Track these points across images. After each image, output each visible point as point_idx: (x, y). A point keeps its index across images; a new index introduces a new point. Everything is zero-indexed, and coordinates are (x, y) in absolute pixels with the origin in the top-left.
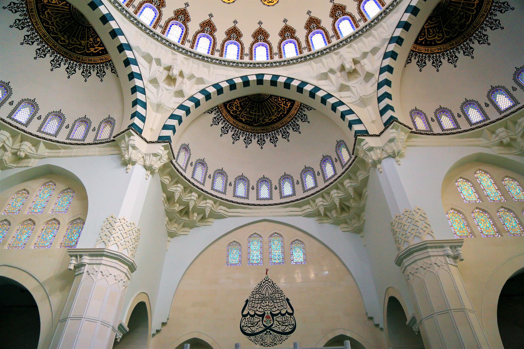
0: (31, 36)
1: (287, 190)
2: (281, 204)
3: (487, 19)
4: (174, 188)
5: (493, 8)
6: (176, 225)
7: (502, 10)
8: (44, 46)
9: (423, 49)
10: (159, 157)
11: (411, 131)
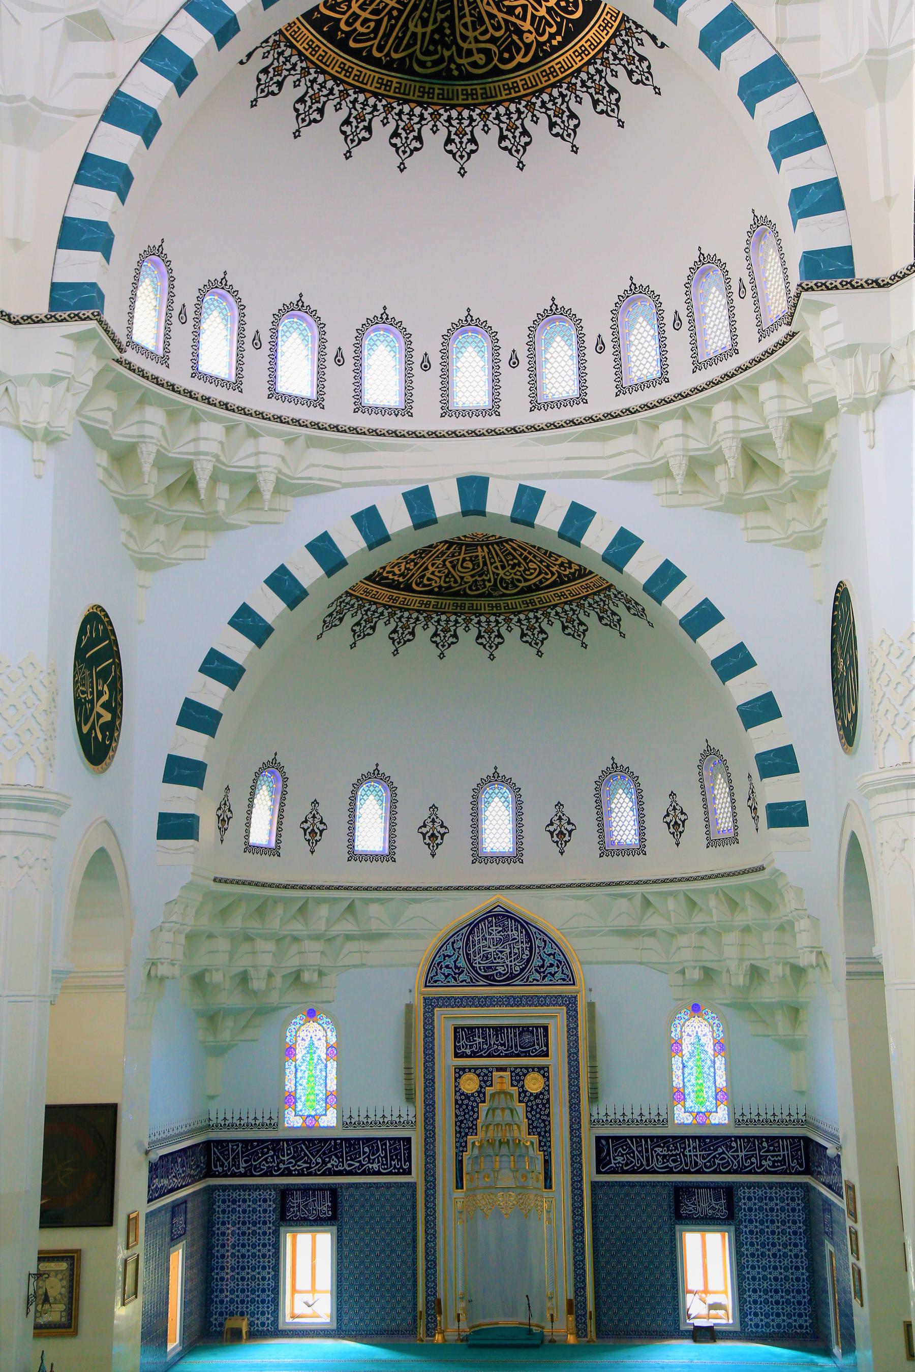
0: (440, 628)
1: (559, 374)
2: (534, 428)
3: (531, 615)
4: (133, 431)
5: (559, 609)
6: (160, 532)
7: (567, 627)
8: (438, 621)
9: (384, 594)
10: (64, 384)
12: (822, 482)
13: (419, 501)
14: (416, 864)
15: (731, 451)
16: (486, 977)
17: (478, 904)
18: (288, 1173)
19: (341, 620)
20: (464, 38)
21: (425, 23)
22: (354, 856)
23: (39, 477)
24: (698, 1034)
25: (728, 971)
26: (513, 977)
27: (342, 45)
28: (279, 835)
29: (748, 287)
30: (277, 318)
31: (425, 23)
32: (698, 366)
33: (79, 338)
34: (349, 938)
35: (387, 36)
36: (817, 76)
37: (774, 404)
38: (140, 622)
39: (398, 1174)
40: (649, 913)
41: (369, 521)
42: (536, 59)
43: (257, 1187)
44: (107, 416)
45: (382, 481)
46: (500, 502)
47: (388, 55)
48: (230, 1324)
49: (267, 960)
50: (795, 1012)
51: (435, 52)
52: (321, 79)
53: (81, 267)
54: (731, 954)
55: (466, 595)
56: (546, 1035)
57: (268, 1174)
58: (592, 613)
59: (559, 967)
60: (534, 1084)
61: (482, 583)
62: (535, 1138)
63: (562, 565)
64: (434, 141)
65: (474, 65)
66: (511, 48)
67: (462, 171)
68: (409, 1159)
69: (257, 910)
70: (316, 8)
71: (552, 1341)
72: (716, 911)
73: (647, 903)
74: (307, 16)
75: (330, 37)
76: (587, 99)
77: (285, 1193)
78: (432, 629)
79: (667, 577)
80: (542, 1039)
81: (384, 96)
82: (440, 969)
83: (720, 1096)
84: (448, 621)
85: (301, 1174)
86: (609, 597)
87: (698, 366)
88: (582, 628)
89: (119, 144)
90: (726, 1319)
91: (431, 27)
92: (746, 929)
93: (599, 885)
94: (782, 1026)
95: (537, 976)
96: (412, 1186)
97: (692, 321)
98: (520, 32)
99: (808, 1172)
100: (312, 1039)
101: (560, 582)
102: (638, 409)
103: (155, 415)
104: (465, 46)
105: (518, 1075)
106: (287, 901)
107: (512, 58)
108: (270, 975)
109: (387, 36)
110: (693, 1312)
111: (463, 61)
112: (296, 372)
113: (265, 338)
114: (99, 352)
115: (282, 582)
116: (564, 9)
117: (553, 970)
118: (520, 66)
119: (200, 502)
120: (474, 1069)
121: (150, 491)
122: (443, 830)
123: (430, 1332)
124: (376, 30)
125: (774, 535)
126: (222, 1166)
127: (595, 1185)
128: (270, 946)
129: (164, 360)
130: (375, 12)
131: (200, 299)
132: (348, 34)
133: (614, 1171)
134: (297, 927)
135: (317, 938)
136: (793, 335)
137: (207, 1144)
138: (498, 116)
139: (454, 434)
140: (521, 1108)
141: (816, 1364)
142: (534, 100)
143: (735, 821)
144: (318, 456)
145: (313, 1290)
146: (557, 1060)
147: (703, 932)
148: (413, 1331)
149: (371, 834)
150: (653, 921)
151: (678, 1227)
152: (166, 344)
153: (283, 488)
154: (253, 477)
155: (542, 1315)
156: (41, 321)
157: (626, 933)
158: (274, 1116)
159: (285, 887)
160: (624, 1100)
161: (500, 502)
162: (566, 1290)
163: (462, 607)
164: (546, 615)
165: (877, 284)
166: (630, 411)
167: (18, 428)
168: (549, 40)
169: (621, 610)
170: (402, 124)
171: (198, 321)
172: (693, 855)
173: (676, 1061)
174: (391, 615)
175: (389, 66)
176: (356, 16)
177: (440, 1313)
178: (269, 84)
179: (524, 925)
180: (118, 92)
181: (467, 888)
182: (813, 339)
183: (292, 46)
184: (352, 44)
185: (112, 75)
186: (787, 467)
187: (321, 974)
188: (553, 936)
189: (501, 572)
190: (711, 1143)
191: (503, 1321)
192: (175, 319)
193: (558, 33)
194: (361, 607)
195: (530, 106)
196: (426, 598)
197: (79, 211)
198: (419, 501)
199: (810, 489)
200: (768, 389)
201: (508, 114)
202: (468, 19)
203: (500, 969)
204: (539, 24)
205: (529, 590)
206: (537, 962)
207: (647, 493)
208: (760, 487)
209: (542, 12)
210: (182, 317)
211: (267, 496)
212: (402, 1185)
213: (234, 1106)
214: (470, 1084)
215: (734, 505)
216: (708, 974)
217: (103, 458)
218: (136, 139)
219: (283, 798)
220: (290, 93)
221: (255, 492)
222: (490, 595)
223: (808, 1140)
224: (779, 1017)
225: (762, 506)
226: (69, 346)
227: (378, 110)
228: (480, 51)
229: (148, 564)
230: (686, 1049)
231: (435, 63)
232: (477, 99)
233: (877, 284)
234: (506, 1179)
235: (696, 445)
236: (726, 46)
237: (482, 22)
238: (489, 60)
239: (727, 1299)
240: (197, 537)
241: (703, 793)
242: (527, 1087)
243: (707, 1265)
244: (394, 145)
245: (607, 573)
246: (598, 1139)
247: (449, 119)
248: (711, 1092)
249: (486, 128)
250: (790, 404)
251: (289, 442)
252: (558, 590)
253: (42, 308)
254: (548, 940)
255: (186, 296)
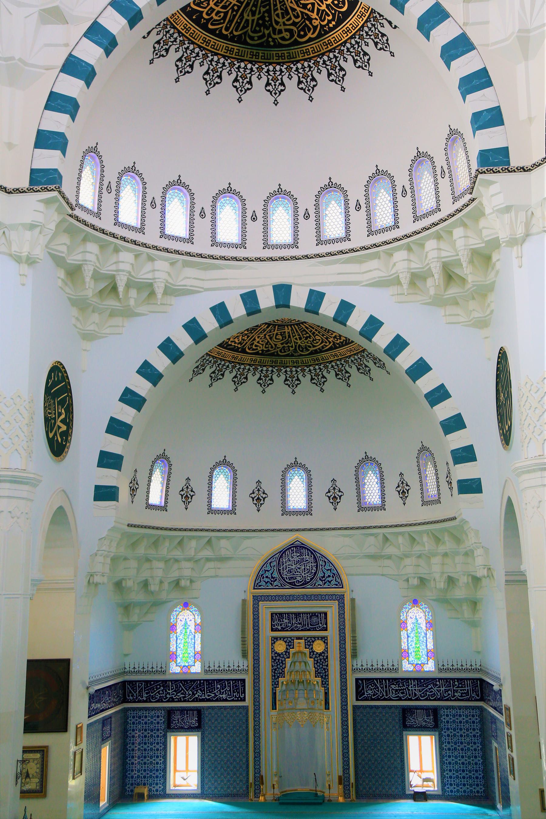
0: (263, 375)
2: (318, 256)
3: (317, 367)
4: (79, 257)
5: (334, 364)
6: (96, 317)
7: (338, 374)
8: (262, 371)
9: (229, 354)
10: (38, 229)
11: (70, 212)
12: (490, 288)
13: (250, 299)
14: (248, 516)
15: (436, 269)
16: (290, 583)
17: (285, 540)
18: (172, 700)
19: (203, 370)
20: (277, 23)
21: (254, 14)
22: (211, 511)
23: (23, 285)
24: (416, 617)
25: (434, 580)
26: (306, 583)
27: (204, 27)
28: (166, 499)
29: (447, 171)
30: (165, 190)
31: (254, 14)
32: (416, 219)
33: (47, 202)
34: (208, 560)
35: (231, 21)
36: (487, 45)
37: (462, 241)
38: (84, 371)
39: (238, 701)
40: (387, 545)
41: (220, 311)
42: (320, 35)
43: (154, 709)
44: (64, 249)
45: (228, 287)
46: (298, 300)
47: (231, 33)
48: (137, 790)
49: (159, 573)
50: (474, 604)
51: (260, 31)
52: (191, 47)
53: (48, 159)
54: (436, 569)
55: (278, 355)
56: (326, 618)
57: (160, 701)
58: (354, 366)
59: (333, 577)
60: (319, 647)
61: (287, 348)
62: (319, 679)
63: (335, 337)
64: (259, 84)
65: (283, 39)
66: (305, 29)
67: (276, 102)
68: (244, 692)
69: (153, 543)
70: (189, 5)
71: (330, 801)
72: (427, 544)
73: (386, 539)
74: (183, 9)
75: (197, 22)
76: (350, 59)
77: (170, 712)
78: (258, 376)
79: (398, 345)
80: (323, 620)
81: (229, 57)
82: (263, 579)
83: (430, 654)
84: (267, 371)
85: (179, 701)
86: (363, 356)
87: (416, 219)
88: (347, 375)
89: (71, 86)
90: (433, 787)
91: (257, 16)
92: (445, 555)
93: (357, 528)
94: (467, 612)
95: (321, 583)
96: (246, 708)
97: (413, 192)
98: (310, 19)
99: (482, 699)
100: (186, 620)
101: (334, 347)
102: (381, 244)
103: (93, 248)
104: (278, 27)
105: (309, 642)
106: (171, 538)
107: (306, 35)
108: (161, 582)
109: (231, 21)
110: (413, 783)
111: (277, 37)
112: (177, 222)
113: (158, 202)
114: (59, 210)
115: (168, 348)
116: (337, 6)
117: (330, 579)
118: (310, 40)
119: (119, 300)
120: (283, 638)
121: (90, 293)
122: (264, 496)
123: (257, 795)
124: (224, 18)
125: (462, 319)
126: (133, 696)
127: (355, 708)
128: (161, 565)
129: (98, 215)
130: (224, 7)
131: (120, 178)
132: (208, 20)
133: (366, 699)
134: (177, 553)
135: (189, 560)
136: (473, 200)
137: (124, 683)
138: (297, 69)
139: (271, 259)
140: (311, 661)
141: (487, 814)
142: (319, 60)
143: (439, 490)
144: (190, 272)
145: (187, 770)
146: (332, 633)
147: (419, 557)
148: (246, 795)
149: (221, 498)
150: (390, 550)
151: (404, 733)
152: (99, 205)
153: (169, 291)
154: (151, 285)
155: (324, 785)
156: (24, 192)
157: (373, 557)
158: (164, 666)
159: (170, 529)
160: (372, 657)
161: (298, 300)
162: (338, 770)
163: (276, 362)
164: (326, 367)
165: (523, 169)
166: (376, 246)
167: (11, 255)
168: (328, 24)
169: (371, 364)
170: (240, 74)
171: (118, 191)
172: (413, 510)
173: (404, 634)
174: (233, 367)
175: (232, 39)
176: (212, 10)
177: (263, 784)
178: (160, 50)
179: (312, 552)
180: (70, 55)
181: (279, 530)
182: (485, 202)
183: (174, 28)
184: (210, 27)
185: (67, 45)
186: (470, 279)
187: (191, 581)
188: (330, 559)
189: (299, 342)
190: (424, 682)
191: (300, 789)
192: (104, 191)
193: (333, 19)
194: (215, 362)
195: (316, 63)
196: (254, 357)
197: (47, 126)
198: (250, 299)
199: (484, 292)
200: (458, 232)
201: (303, 68)
202: (279, 12)
203: (298, 579)
204: (322, 14)
205: (316, 352)
206: (320, 574)
207: (386, 294)
208: (454, 291)
209: (324, 7)
210: (108, 189)
211: (159, 296)
212: (240, 707)
213: (140, 660)
214: (280, 647)
215: (438, 302)
216: (423, 581)
217: (62, 274)
218: (81, 83)
219: (169, 476)
220: (173, 56)
221: (152, 294)
222: (292, 355)
223: (482, 681)
224: (465, 607)
225: (455, 302)
226: (41, 207)
227: (226, 66)
228: (286, 30)
229: (88, 337)
230: (410, 626)
231: (260, 38)
232: (285, 59)
233: (523, 169)
234: (302, 704)
235: (416, 265)
236: (433, 27)
237: (288, 13)
238: (292, 36)
239: (434, 776)
240: (118, 321)
241: (420, 473)
242: (314, 649)
243: (422, 755)
244: (235, 87)
245: (362, 342)
246: (357, 680)
247: (268, 71)
248: (425, 652)
249: (290, 77)
250: (471, 241)
251: (172, 264)
252: (333, 352)
253: (25, 184)
254: (327, 561)
255: (111, 177)
